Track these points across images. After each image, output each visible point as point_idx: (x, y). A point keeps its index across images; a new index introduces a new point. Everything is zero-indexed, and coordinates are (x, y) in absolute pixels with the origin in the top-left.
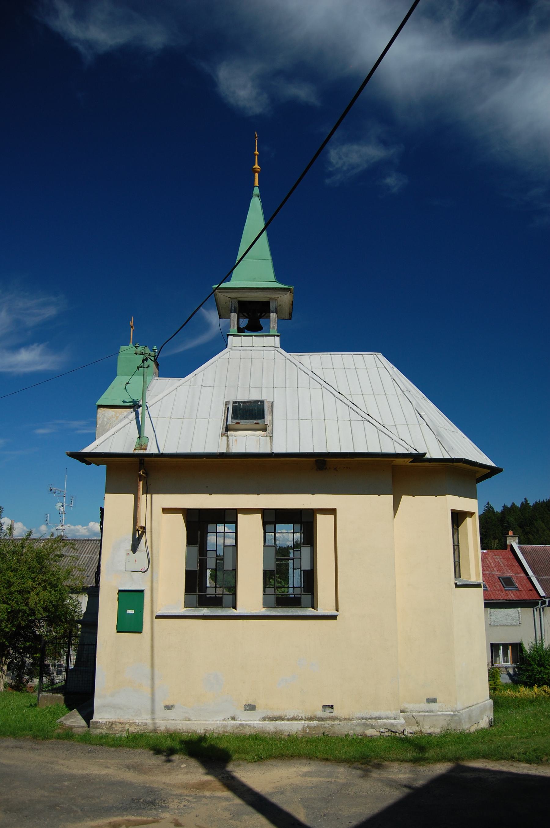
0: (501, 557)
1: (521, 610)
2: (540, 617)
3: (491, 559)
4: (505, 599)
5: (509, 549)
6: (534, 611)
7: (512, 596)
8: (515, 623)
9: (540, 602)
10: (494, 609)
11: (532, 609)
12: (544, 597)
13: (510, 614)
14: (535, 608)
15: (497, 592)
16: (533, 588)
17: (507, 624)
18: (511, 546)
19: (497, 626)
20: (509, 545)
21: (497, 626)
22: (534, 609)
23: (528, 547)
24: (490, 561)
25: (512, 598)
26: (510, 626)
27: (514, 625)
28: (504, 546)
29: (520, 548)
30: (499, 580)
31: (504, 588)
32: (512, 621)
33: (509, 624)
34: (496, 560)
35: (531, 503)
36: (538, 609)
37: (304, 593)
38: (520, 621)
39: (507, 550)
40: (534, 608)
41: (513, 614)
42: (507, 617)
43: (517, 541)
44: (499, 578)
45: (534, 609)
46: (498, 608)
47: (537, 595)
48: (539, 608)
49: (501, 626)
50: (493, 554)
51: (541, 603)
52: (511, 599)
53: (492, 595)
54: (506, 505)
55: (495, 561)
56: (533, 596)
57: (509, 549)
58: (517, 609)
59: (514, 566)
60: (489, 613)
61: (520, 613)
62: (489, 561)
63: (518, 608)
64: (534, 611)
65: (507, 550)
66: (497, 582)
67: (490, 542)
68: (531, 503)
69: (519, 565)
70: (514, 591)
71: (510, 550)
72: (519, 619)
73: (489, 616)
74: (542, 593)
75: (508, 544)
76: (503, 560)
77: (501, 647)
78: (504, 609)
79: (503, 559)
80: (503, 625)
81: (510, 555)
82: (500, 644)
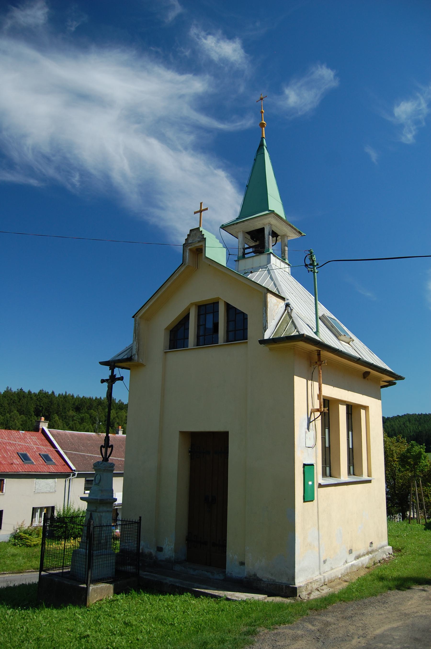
0: (36, 437)
1: (57, 480)
2: (69, 484)
3: (30, 439)
4: (49, 471)
5: (40, 431)
6: (66, 481)
7: (52, 469)
8: (52, 491)
9: (72, 474)
10: (38, 480)
11: (64, 479)
12: (74, 470)
13: (49, 484)
14: (67, 479)
15: (42, 466)
16: (65, 464)
17: (46, 492)
18: (43, 429)
19: (39, 493)
20: (41, 429)
21: (39, 493)
22: (66, 480)
23: (54, 431)
24: (29, 440)
25: (53, 471)
26: (48, 493)
27: (51, 492)
28: (36, 429)
29: (49, 431)
30: (40, 456)
31: (46, 462)
32: (50, 489)
33: (48, 492)
34: (34, 440)
35: (57, 394)
36: (69, 480)
37: (324, 474)
38: (55, 489)
39: (38, 432)
40: (67, 479)
41: (51, 484)
42: (47, 486)
43: (47, 425)
44: (40, 454)
45: (66, 480)
46: (41, 479)
47: (69, 469)
48: (69, 479)
49: (42, 493)
50: (30, 435)
51: (72, 475)
52: (53, 472)
53: (39, 469)
54: (22, 389)
55: (33, 440)
56: (65, 470)
57: (41, 432)
58: (54, 479)
59: (47, 445)
60: (35, 483)
61: (56, 483)
62: (28, 440)
63: (55, 479)
64: (66, 481)
65: (38, 432)
66: (39, 458)
67: (12, 419)
68: (57, 394)
69: (50, 445)
70: (53, 465)
71: (42, 432)
72: (55, 488)
73: (35, 485)
74: (74, 468)
75: (41, 427)
76: (38, 440)
77: (39, 510)
78: (46, 479)
79: (38, 439)
80: (43, 493)
81: (42, 437)
82: (38, 507)
